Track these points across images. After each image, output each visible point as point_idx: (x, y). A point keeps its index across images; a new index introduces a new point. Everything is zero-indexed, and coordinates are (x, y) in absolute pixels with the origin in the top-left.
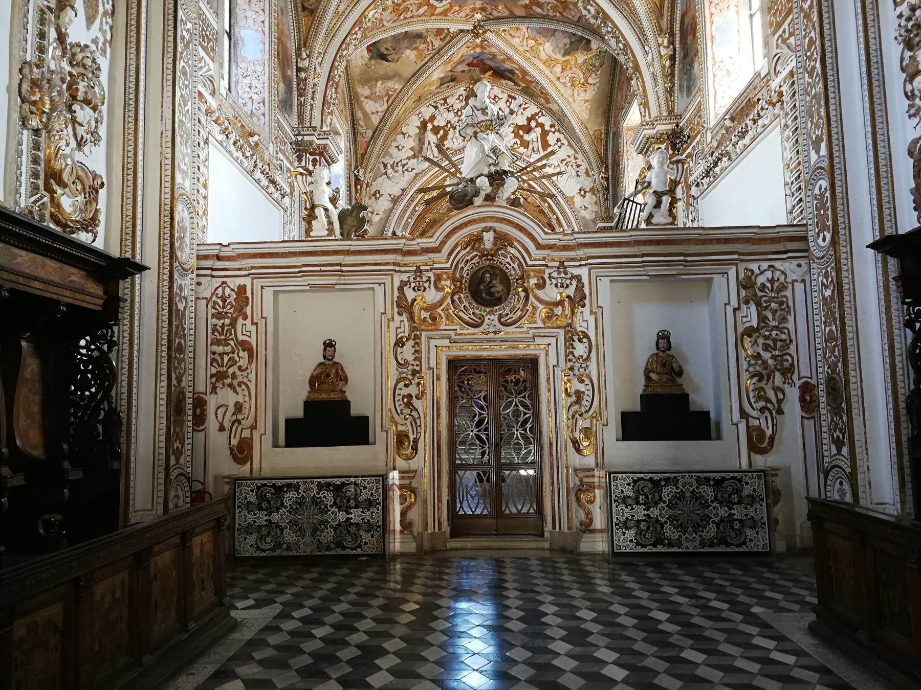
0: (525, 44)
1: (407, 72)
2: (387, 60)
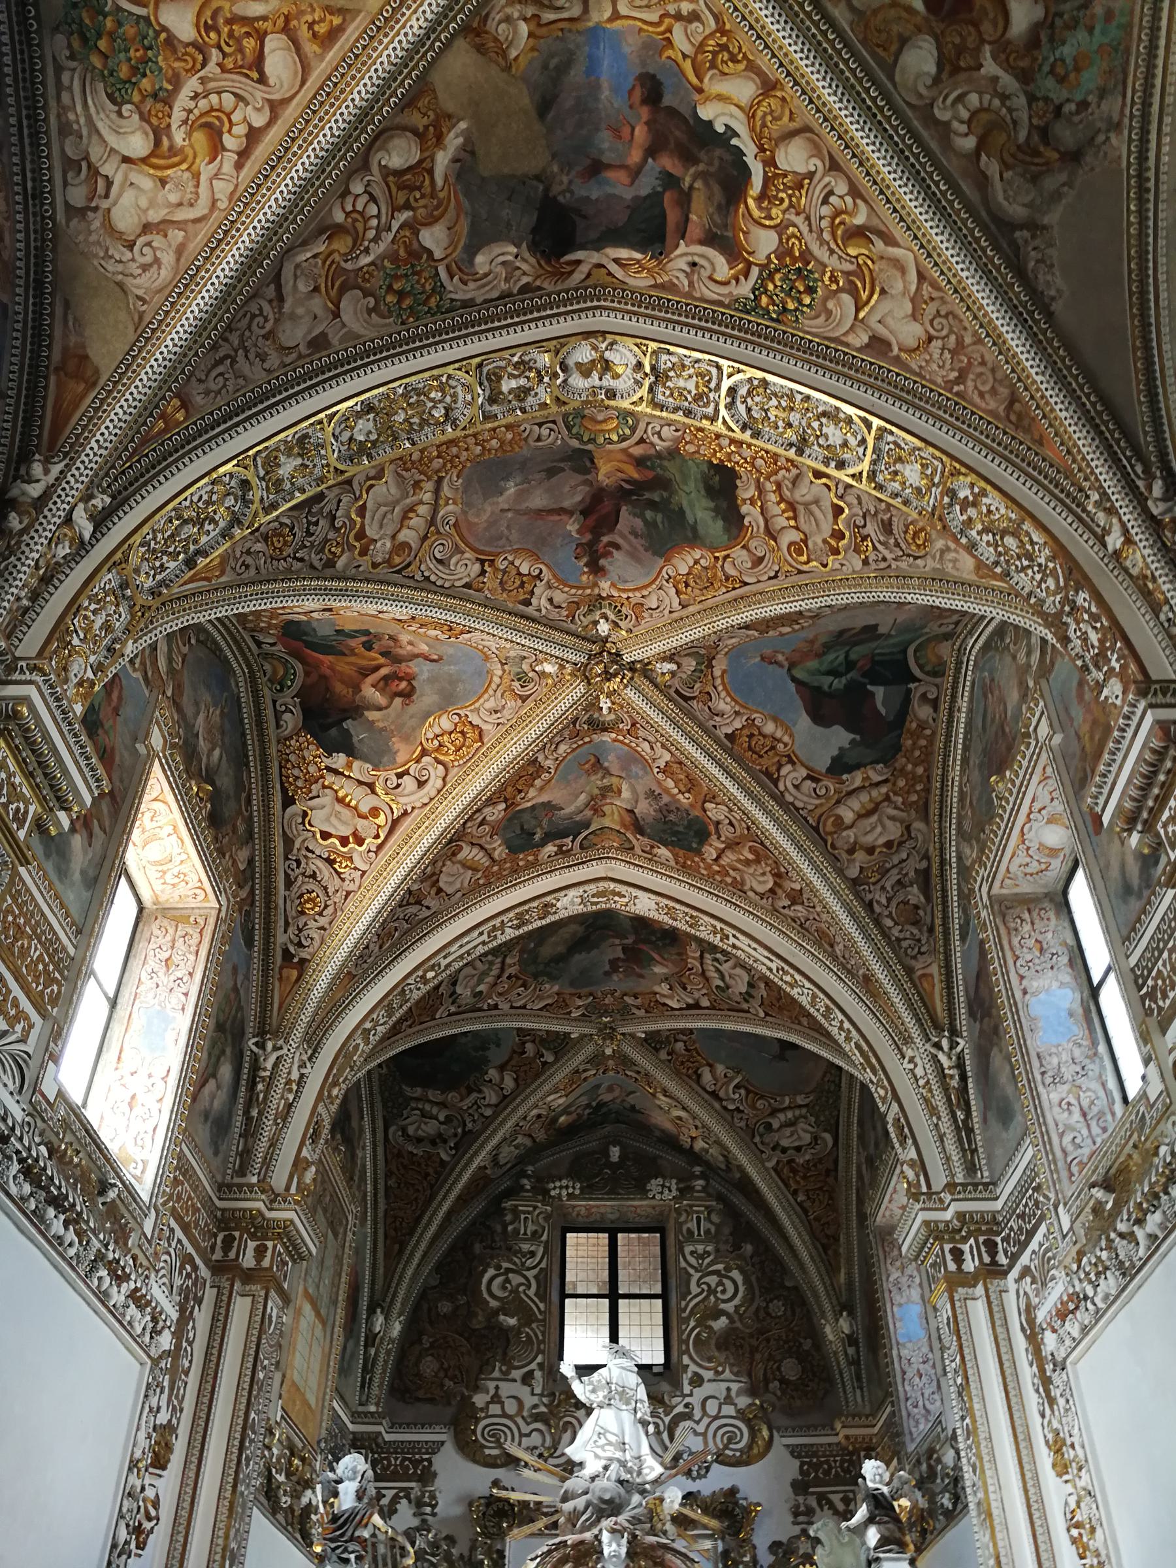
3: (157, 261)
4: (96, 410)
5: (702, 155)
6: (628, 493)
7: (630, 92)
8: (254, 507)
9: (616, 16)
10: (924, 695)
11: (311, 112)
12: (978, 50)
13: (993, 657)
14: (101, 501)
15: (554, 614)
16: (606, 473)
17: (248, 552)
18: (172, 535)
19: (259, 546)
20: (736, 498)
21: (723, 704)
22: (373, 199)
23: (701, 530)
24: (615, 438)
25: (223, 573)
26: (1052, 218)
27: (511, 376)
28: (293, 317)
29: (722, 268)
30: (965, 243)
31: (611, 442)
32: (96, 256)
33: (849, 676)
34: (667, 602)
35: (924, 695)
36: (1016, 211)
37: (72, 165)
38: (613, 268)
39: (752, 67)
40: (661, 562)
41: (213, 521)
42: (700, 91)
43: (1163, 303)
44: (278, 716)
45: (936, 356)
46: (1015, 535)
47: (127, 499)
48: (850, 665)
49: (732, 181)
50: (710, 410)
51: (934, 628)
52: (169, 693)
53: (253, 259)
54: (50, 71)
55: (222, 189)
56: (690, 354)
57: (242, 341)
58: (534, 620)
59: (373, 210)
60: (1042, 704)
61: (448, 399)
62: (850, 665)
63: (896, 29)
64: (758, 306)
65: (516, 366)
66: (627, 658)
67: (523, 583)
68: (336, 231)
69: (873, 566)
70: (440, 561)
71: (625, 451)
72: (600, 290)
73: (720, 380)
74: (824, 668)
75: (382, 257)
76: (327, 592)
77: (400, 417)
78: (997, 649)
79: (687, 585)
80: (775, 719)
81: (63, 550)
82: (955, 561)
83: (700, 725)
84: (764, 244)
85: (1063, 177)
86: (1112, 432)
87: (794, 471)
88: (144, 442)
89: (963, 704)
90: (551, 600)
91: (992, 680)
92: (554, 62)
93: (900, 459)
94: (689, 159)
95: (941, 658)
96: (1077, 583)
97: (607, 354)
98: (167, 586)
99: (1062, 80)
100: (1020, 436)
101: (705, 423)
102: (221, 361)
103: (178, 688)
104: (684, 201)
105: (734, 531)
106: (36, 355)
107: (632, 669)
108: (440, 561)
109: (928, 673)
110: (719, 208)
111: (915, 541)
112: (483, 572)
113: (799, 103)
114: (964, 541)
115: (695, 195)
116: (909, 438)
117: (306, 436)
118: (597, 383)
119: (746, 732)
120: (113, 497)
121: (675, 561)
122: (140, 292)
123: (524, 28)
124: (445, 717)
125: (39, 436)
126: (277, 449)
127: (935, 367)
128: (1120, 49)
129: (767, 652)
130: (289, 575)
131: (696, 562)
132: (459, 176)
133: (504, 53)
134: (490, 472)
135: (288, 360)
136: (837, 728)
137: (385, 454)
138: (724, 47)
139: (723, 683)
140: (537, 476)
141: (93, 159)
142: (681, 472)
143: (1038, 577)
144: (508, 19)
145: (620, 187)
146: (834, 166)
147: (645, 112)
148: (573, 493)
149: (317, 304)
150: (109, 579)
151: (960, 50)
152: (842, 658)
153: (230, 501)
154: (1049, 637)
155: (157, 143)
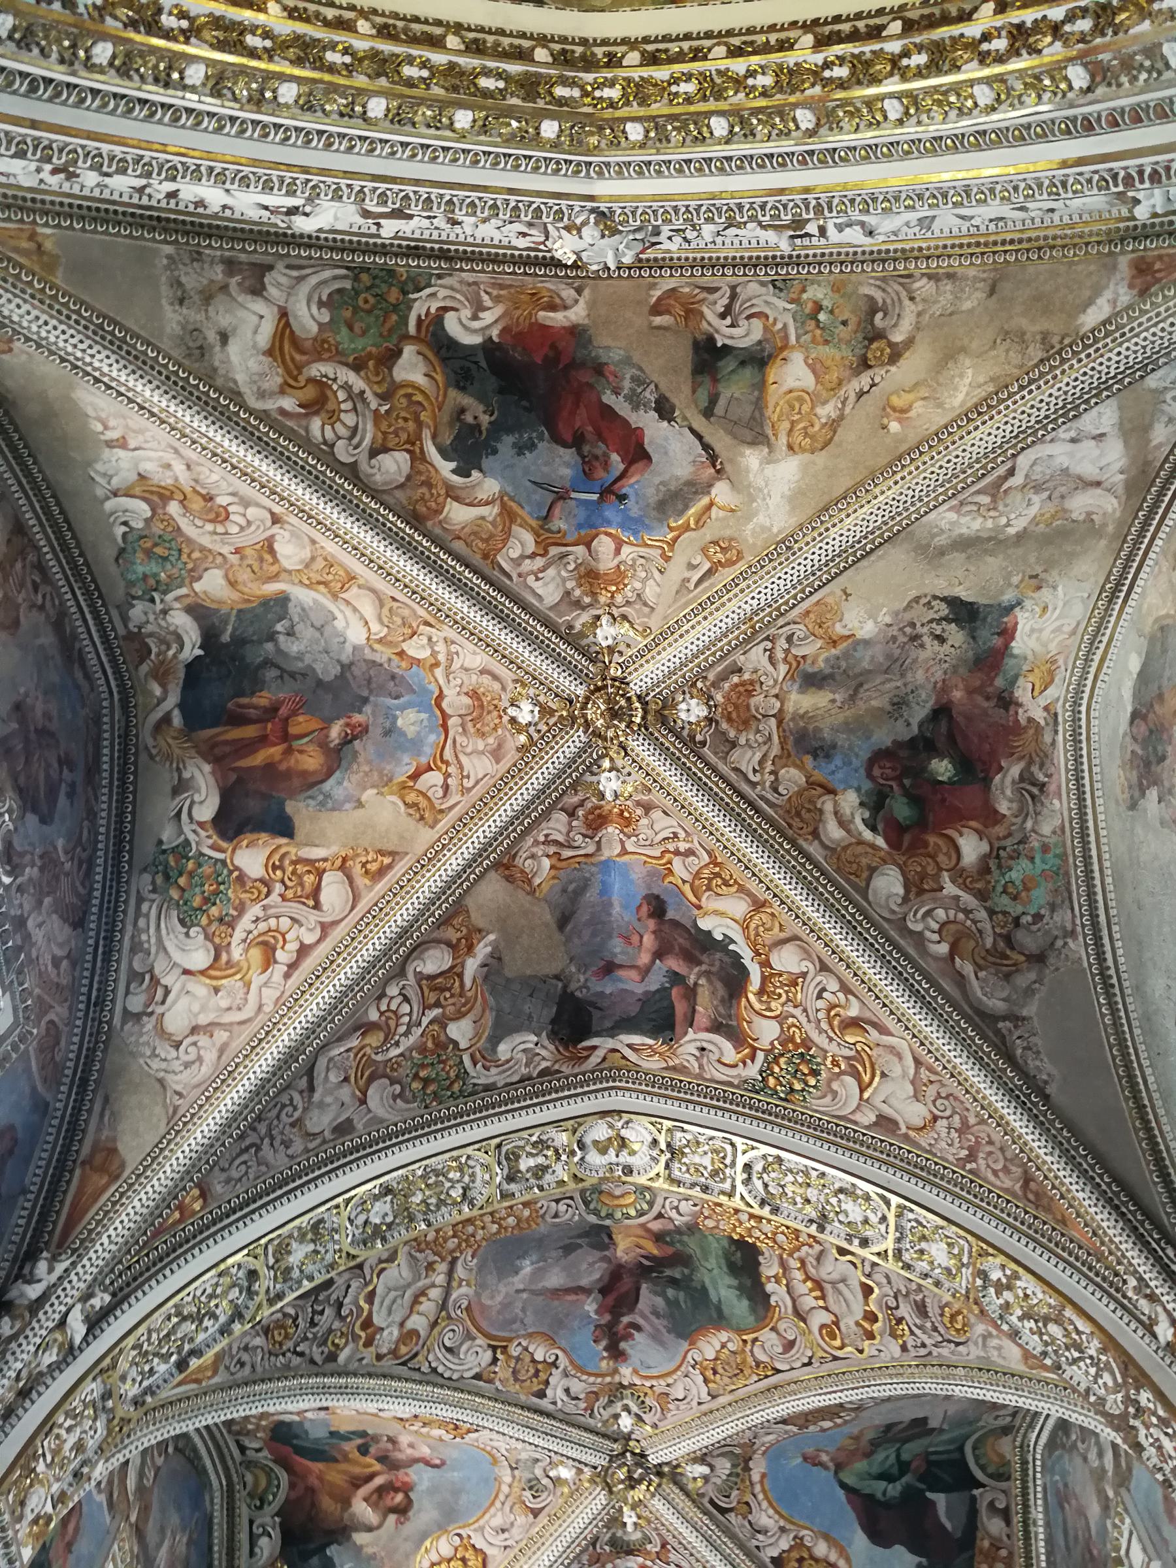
0: (441, 647)
1: (897, 556)
2: (953, 602)
3: (200, 1059)
4: (114, 1204)
5: (704, 958)
6: (648, 1269)
7: (639, 908)
8: (257, 1299)
9: (624, 852)
10: (991, 1504)
11: (358, 929)
12: (937, 877)
13: (1061, 1457)
14: (101, 1300)
15: (571, 1407)
16: (625, 1249)
17: (246, 1348)
18: (168, 1335)
19: (259, 1341)
20: (759, 1275)
21: (765, 1518)
22: (406, 999)
23: (726, 1310)
24: (633, 1213)
25: (215, 1372)
26: (1030, 1010)
27: (529, 1154)
28: (322, 1105)
29: (729, 1052)
30: (954, 1033)
31: (629, 1217)
32: (143, 1055)
33: (904, 1480)
34: (694, 1391)
35: (991, 1504)
36: (996, 1004)
37: (136, 977)
38: (628, 1052)
39: (742, 889)
40: (685, 1345)
41: (214, 1316)
42: (699, 907)
43: (1153, 1087)
44: (253, 1540)
45: (944, 1134)
46: (1058, 1321)
47: (128, 1296)
48: (903, 1467)
49: (733, 980)
50: (727, 1186)
51: (989, 1421)
52: (133, 1519)
53: (291, 1056)
54: (133, 902)
55: (270, 995)
56: (707, 1135)
57: (270, 1129)
58: (548, 1415)
59: (406, 1008)
60: (1128, 1521)
61: (466, 1179)
62: (903, 1467)
63: (864, 861)
64: (766, 1086)
65: (534, 1145)
66: (653, 1460)
67: (537, 1371)
68: (368, 1028)
69: (913, 1353)
70: (449, 1350)
71: (643, 1226)
72: (615, 1072)
73: (735, 1155)
74: (875, 1470)
75: (410, 1049)
76: (325, 1390)
77: (417, 1198)
78: (1063, 1446)
79: (715, 1373)
80: (827, 1537)
81: (50, 1357)
82: (999, 1348)
83: (742, 1546)
84: (767, 1032)
85: (1032, 976)
86: (1133, 1213)
87: (818, 1248)
88: (155, 1235)
89: (1038, 1514)
90: (567, 1391)
91: (1066, 1485)
92: (571, 888)
93: (923, 1238)
94: (691, 959)
95: (1001, 1456)
96: (1136, 1380)
97: (623, 1132)
98: (153, 1394)
99: (1015, 898)
100: (1042, 1215)
101: (723, 1199)
102: (247, 1149)
103: (145, 1510)
104: (691, 994)
105: (761, 1312)
106: (66, 1149)
107: (660, 1474)
108: (449, 1350)
109: (991, 1476)
110: (722, 1001)
111: (954, 1324)
112: (495, 1360)
113: (786, 917)
114: (1005, 1327)
115: (700, 990)
116: (930, 1216)
117: (321, 1221)
118: (614, 1159)
119: (795, 1555)
120: (114, 1295)
121: (700, 1344)
122: (178, 1088)
123: (546, 863)
124: (443, 1539)
125: (51, 1233)
126: (290, 1236)
127: (943, 1145)
128: (1060, 873)
129: (810, 1450)
130: (286, 1373)
131: (723, 1346)
132: (486, 978)
133: (530, 882)
134: (506, 1250)
135: (311, 1146)
136: (899, 1549)
137: (400, 1235)
138: (717, 875)
139: (764, 1491)
140: (554, 1254)
141: (157, 971)
142: (702, 1248)
143: (1093, 1371)
144: (533, 856)
145: (631, 983)
146: (824, 968)
147: (651, 924)
148: (590, 1269)
149: (345, 1093)
150: (92, 1389)
151: (923, 876)
152: (893, 1458)
153: (235, 1293)
154: (1119, 1441)
155: (217, 957)
